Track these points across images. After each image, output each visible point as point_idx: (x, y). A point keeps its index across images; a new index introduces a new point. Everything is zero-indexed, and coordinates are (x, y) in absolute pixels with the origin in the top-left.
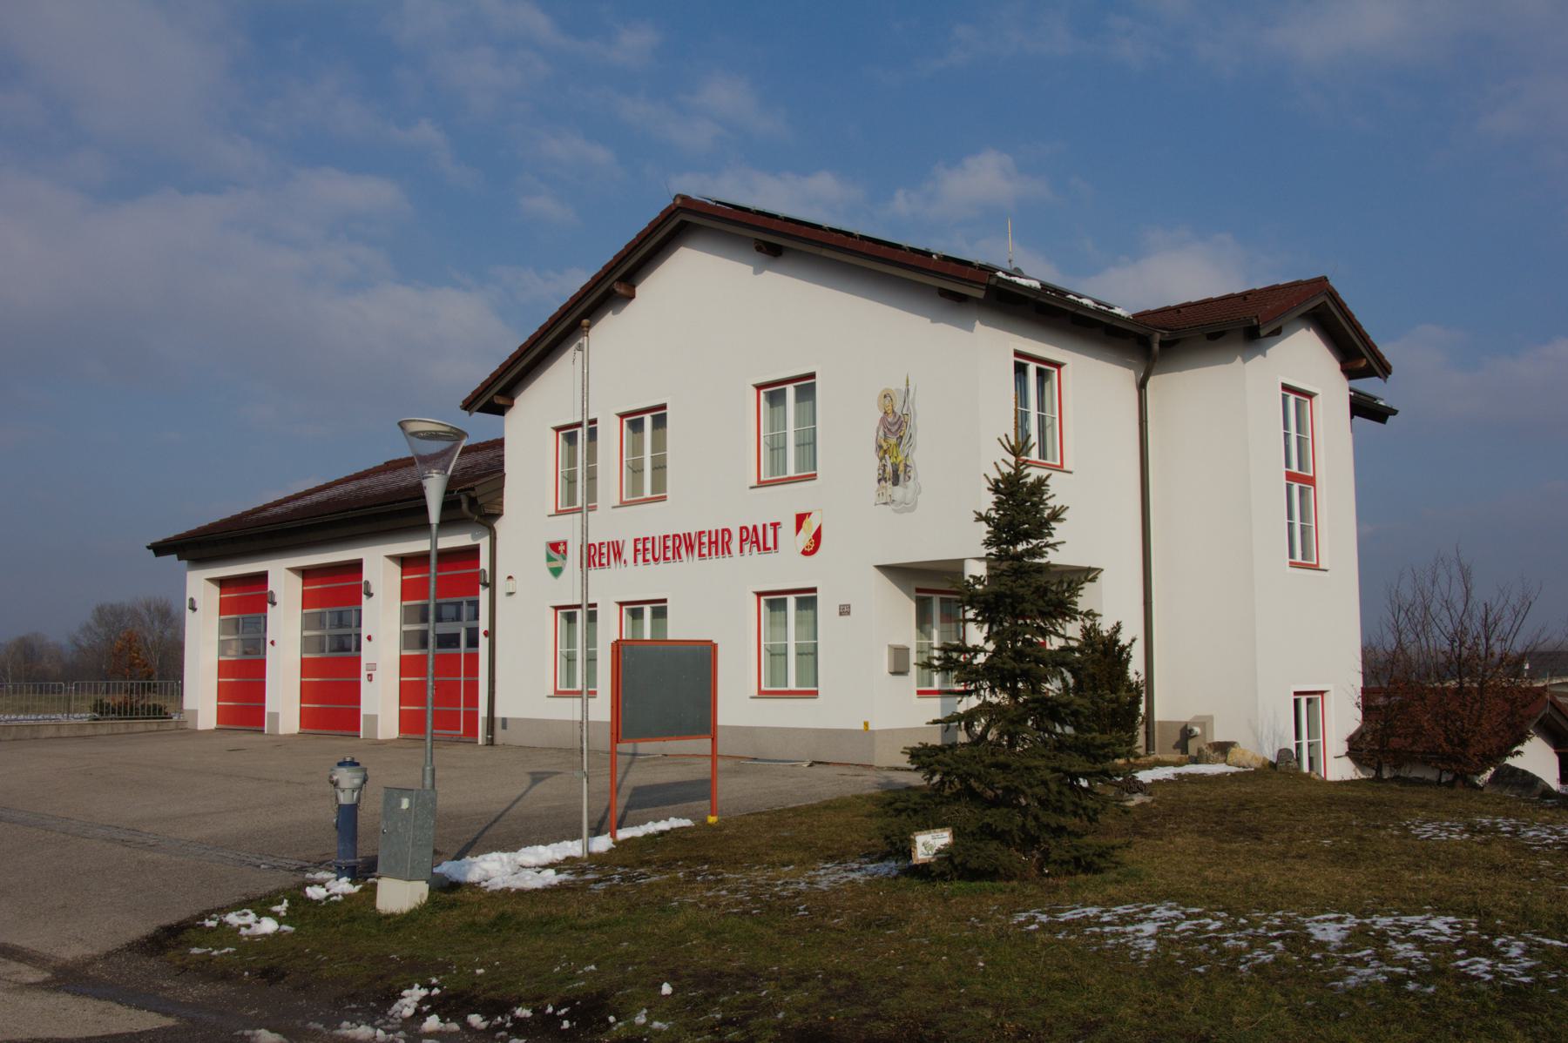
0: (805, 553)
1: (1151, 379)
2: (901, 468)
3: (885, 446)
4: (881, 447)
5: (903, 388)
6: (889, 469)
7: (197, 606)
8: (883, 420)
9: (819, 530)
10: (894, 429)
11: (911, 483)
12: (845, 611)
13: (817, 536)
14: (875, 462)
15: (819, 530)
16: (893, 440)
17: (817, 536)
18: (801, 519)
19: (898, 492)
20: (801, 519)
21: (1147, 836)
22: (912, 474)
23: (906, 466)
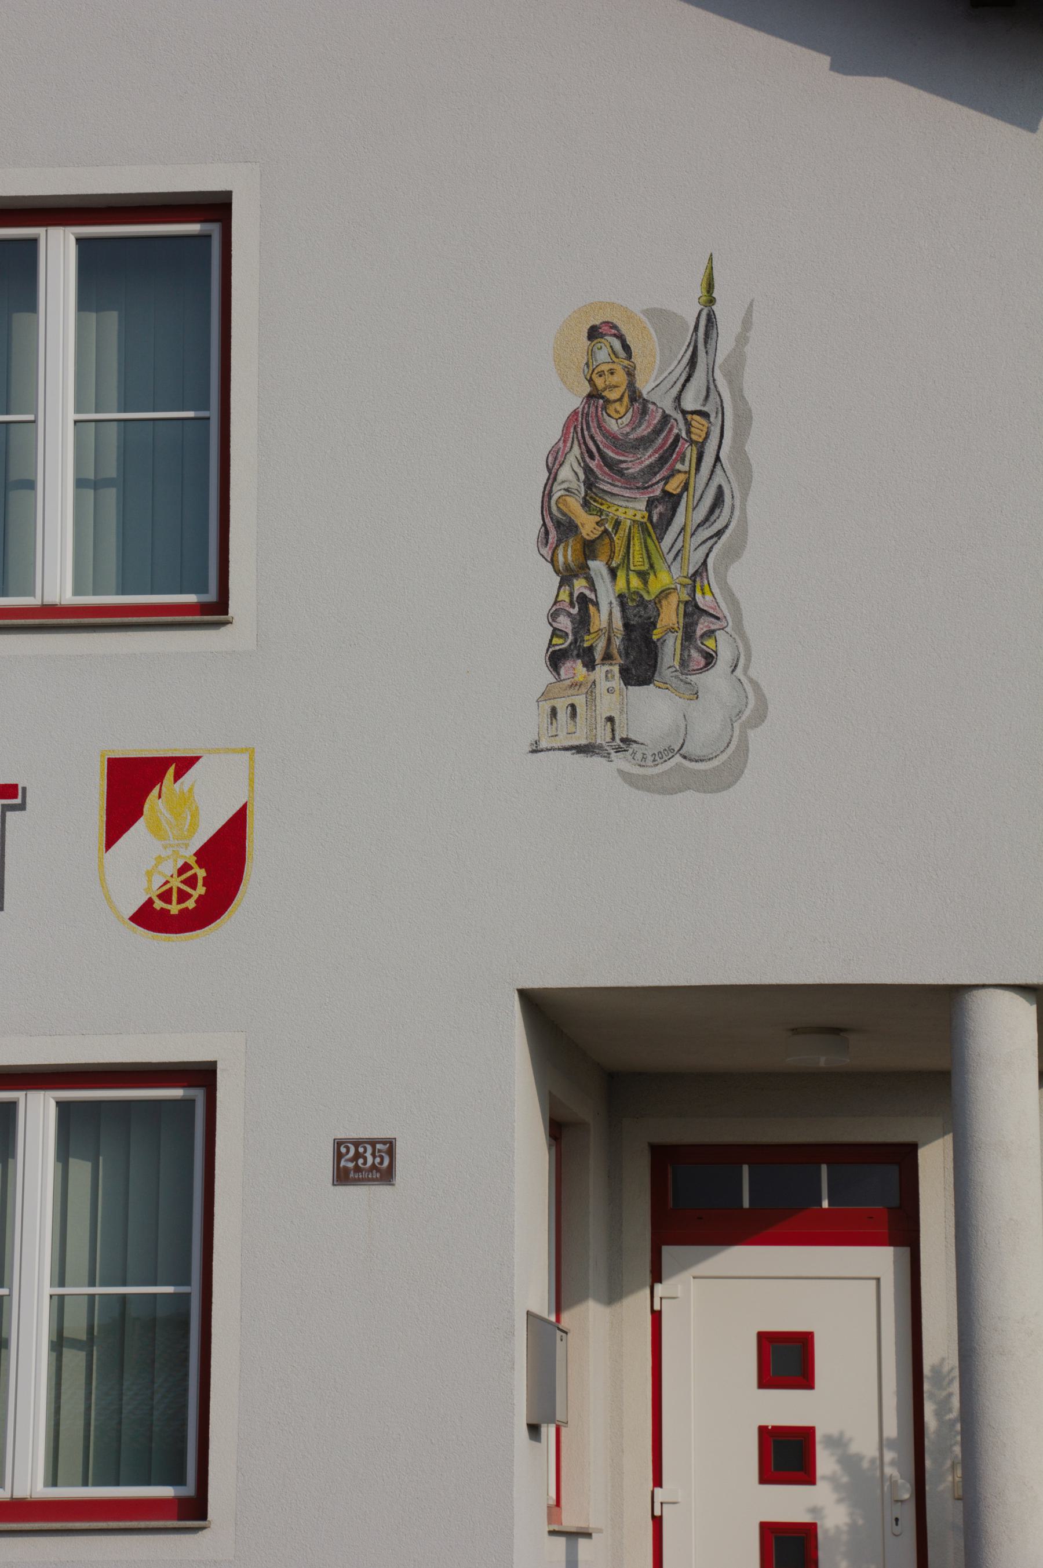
0: (148, 918)
1: (730, 580)
2: (670, 616)
3: (588, 525)
4: (566, 528)
5: (689, 310)
6: (607, 615)
7: (775, 567)
8: (580, 425)
9: (236, 828)
10: (636, 464)
11: (715, 682)
12: (364, 1163)
13: (224, 858)
14: (542, 584)
15: (236, 828)
16: (631, 508)
17: (224, 858)
18: (131, 786)
19: (652, 710)
20: (131, 786)
21: (626, 309)
22: (724, 648)
23: (693, 612)
